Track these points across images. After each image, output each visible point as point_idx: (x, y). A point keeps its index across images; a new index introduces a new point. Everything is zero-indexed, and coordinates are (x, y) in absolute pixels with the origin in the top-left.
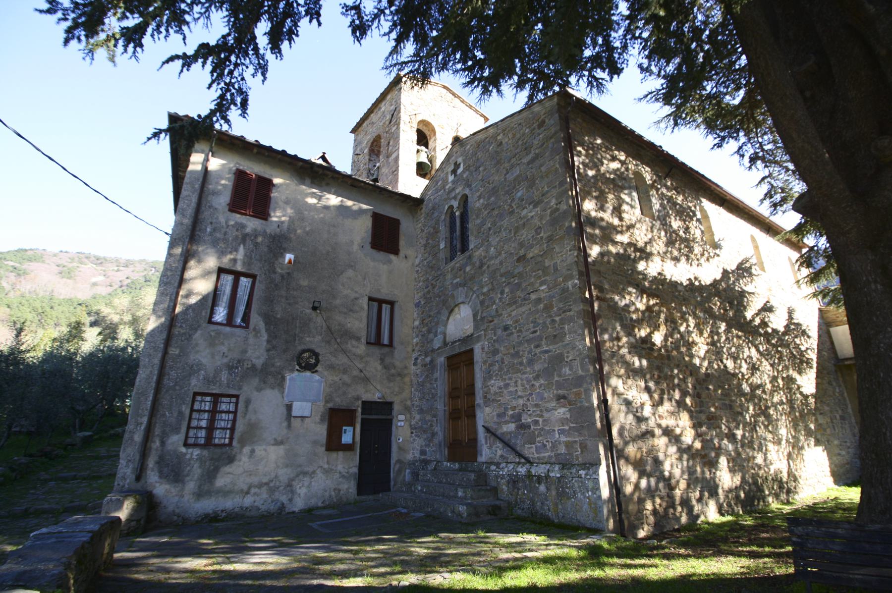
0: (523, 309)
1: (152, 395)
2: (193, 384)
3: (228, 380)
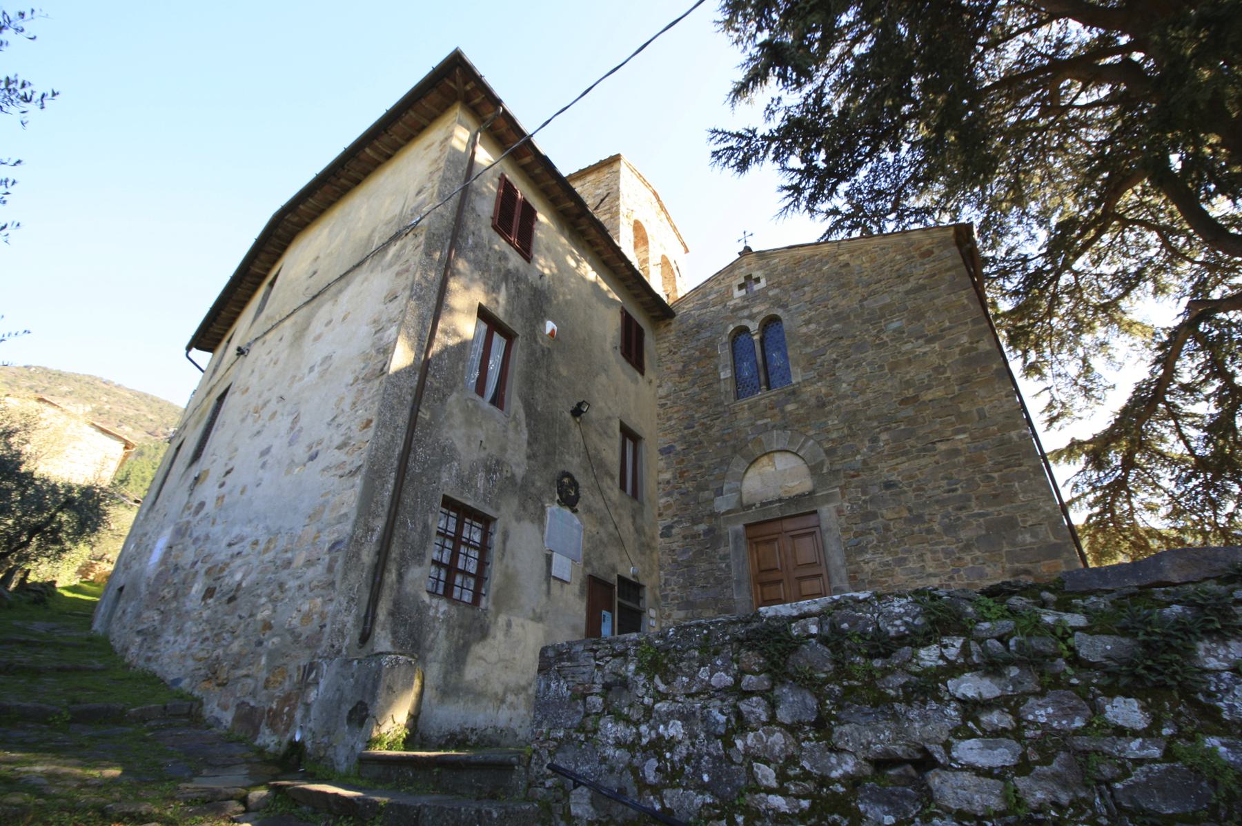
0: (923, 461)
1: (392, 481)
2: (444, 480)
3: (485, 490)
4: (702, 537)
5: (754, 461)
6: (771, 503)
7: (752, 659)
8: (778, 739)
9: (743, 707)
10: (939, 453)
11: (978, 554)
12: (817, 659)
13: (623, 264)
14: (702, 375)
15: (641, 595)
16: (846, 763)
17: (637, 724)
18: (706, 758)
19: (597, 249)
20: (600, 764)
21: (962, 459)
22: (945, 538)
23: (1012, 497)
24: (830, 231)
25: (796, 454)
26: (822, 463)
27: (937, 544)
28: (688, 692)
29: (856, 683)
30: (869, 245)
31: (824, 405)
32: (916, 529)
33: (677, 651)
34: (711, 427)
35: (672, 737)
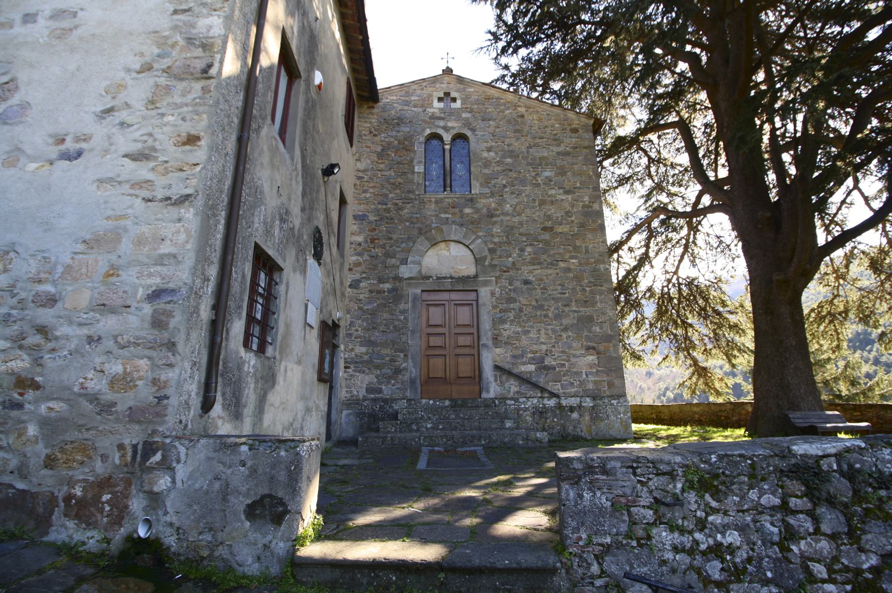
0: (549, 271)
1: (223, 222)
4: (386, 294)
5: (435, 244)
6: (445, 278)
7: (796, 487)
8: (824, 545)
9: (791, 520)
10: (560, 268)
11: (571, 334)
12: (841, 487)
13: (361, 37)
14: (399, 163)
15: (337, 333)
16: (871, 559)
17: (691, 533)
18: (767, 559)
19: (344, 10)
20: (660, 565)
21: (571, 275)
22: (554, 322)
23: (594, 304)
24: (497, 80)
25: (467, 247)
26: (485, 258)
27: (549, 325)
28: (741, 508)
29: (871, 506)
30: (540, 107)
31: (492, 216)
32: (538, 313)
33: (727, 476)
34: (402, 209)
35: (731, 544)
